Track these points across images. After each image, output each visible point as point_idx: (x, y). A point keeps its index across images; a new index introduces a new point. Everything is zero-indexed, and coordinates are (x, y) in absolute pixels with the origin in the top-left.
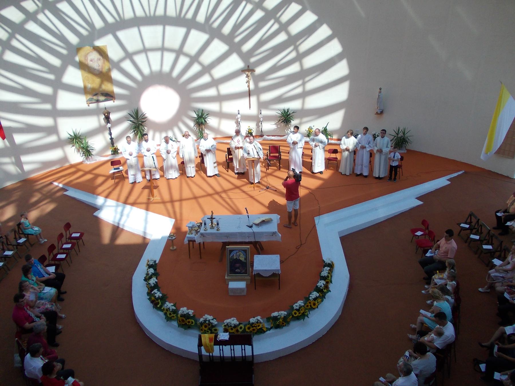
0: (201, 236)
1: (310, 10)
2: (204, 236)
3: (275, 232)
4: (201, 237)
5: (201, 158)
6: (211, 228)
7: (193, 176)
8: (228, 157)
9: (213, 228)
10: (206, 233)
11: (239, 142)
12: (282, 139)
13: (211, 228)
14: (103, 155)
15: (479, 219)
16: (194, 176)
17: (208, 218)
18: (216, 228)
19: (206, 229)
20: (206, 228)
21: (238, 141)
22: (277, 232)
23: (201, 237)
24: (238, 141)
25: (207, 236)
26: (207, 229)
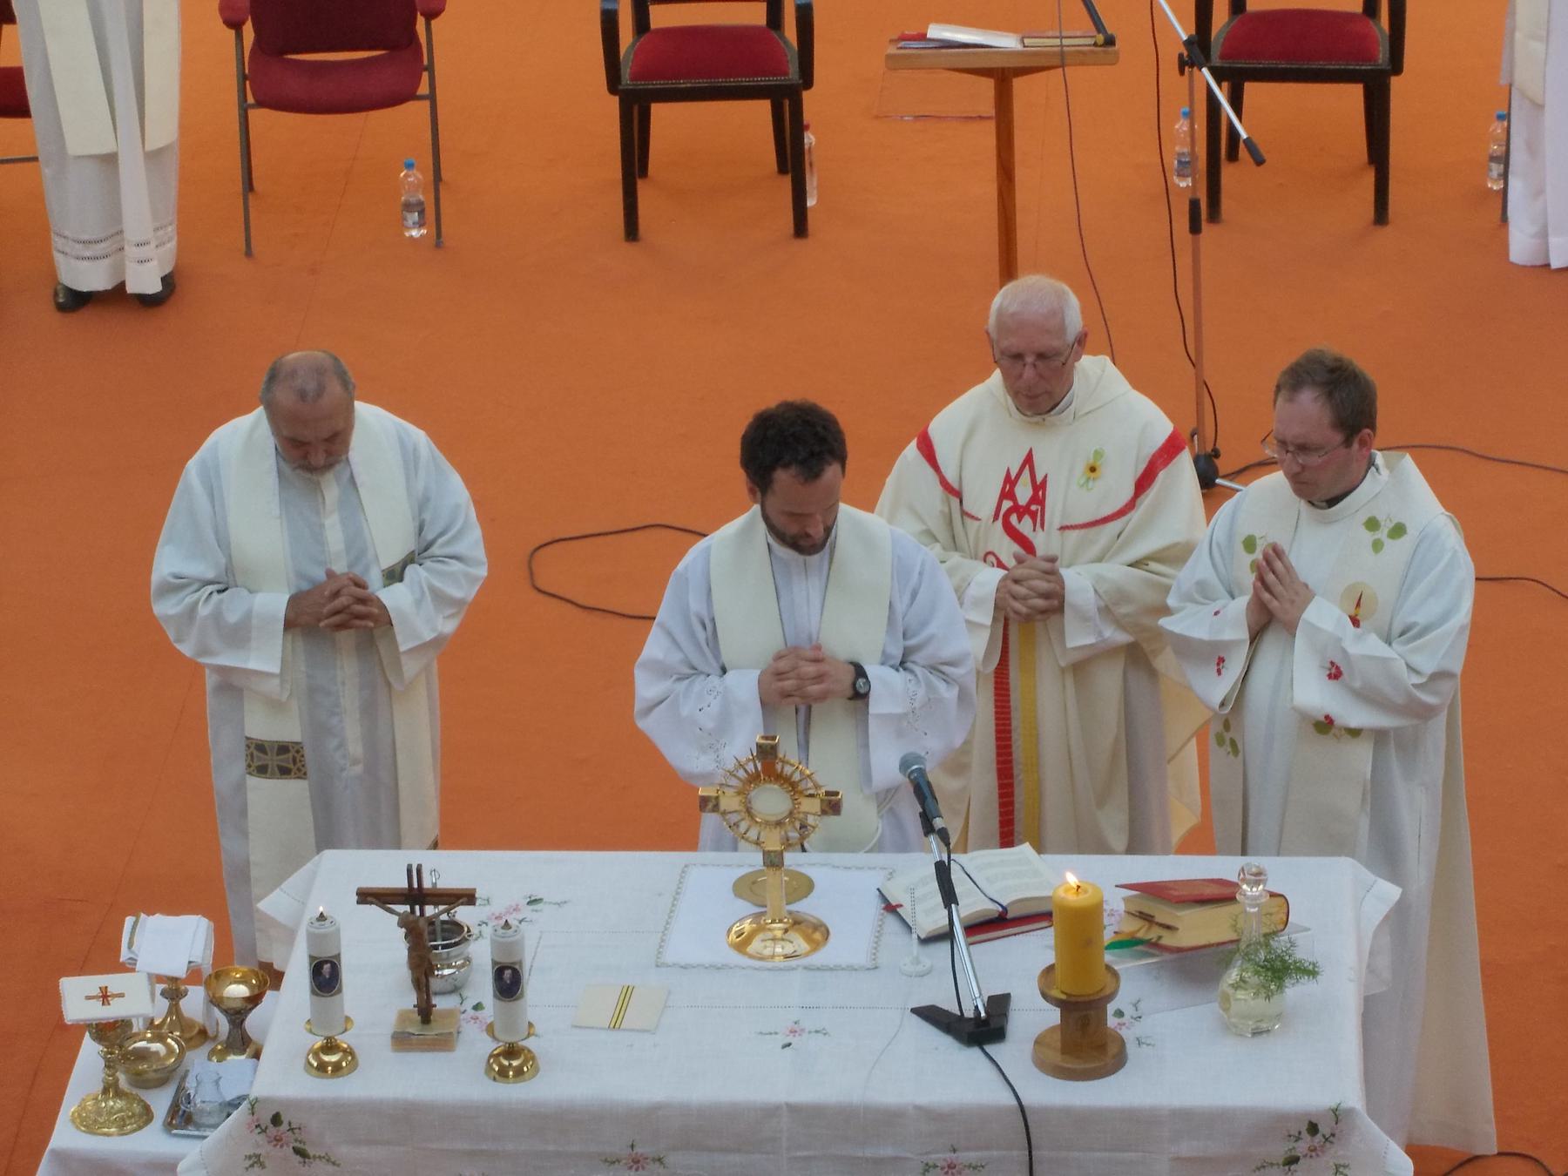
0: (265, 1149)
1: (1297, 578)
2: (300, 1152)
3: (1337, 1114)
4: (256, 1161)
5: (249, 31)
6: (402, 1041)
7: (153, 286)
8: (642, 24)
9: (444, 1043)
10: (340, 1112)
11: (1025, 526)
12: (1382, 20)
13: (402, 1041)
14: (388, 674)
15: (220, 1078)
16: (167, 281)
17: (365, 896)
18: (476, 1045)
19: (330, 1047)
20: (344, 1041)
21: (1023, 493)
22: (1350, 1112)
23: (256, 1161)
24: (1023, 493)
25: (343, 1151)
26: (349, 1052)
